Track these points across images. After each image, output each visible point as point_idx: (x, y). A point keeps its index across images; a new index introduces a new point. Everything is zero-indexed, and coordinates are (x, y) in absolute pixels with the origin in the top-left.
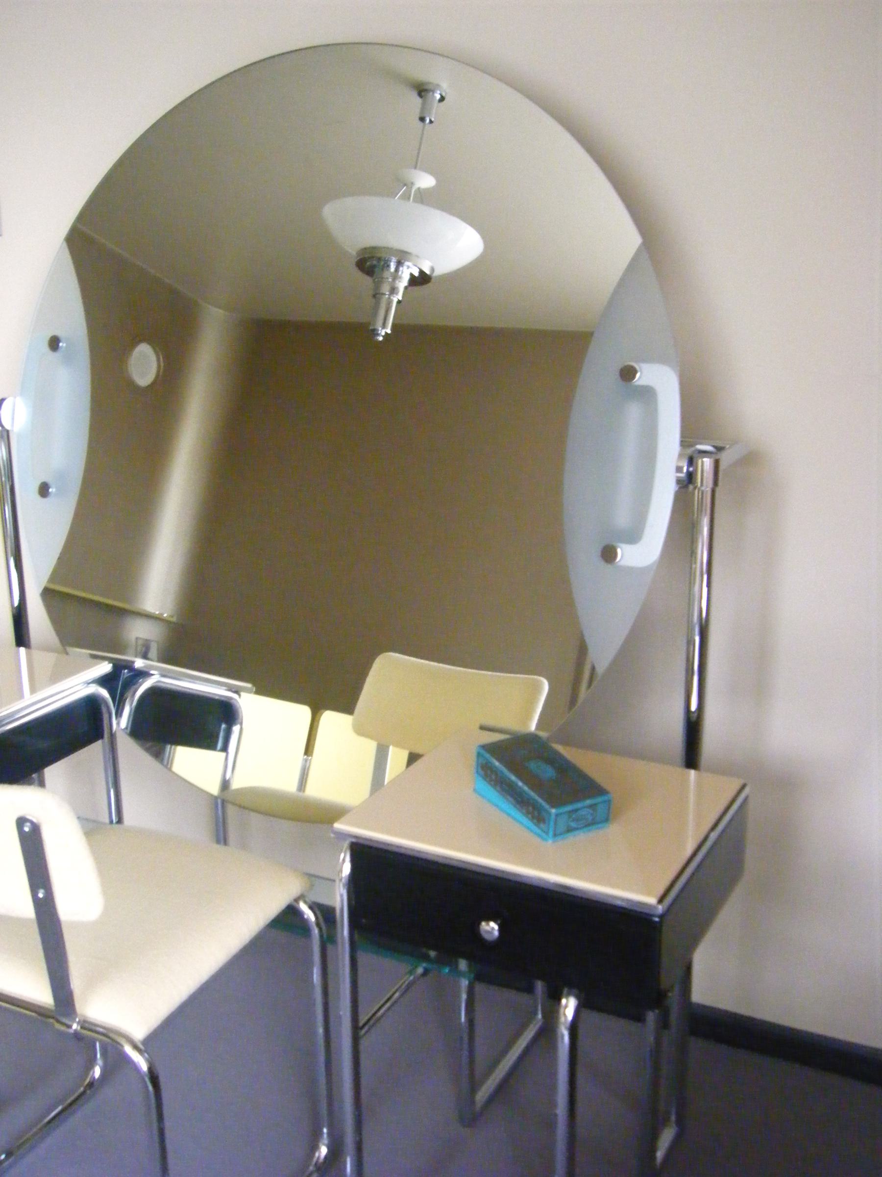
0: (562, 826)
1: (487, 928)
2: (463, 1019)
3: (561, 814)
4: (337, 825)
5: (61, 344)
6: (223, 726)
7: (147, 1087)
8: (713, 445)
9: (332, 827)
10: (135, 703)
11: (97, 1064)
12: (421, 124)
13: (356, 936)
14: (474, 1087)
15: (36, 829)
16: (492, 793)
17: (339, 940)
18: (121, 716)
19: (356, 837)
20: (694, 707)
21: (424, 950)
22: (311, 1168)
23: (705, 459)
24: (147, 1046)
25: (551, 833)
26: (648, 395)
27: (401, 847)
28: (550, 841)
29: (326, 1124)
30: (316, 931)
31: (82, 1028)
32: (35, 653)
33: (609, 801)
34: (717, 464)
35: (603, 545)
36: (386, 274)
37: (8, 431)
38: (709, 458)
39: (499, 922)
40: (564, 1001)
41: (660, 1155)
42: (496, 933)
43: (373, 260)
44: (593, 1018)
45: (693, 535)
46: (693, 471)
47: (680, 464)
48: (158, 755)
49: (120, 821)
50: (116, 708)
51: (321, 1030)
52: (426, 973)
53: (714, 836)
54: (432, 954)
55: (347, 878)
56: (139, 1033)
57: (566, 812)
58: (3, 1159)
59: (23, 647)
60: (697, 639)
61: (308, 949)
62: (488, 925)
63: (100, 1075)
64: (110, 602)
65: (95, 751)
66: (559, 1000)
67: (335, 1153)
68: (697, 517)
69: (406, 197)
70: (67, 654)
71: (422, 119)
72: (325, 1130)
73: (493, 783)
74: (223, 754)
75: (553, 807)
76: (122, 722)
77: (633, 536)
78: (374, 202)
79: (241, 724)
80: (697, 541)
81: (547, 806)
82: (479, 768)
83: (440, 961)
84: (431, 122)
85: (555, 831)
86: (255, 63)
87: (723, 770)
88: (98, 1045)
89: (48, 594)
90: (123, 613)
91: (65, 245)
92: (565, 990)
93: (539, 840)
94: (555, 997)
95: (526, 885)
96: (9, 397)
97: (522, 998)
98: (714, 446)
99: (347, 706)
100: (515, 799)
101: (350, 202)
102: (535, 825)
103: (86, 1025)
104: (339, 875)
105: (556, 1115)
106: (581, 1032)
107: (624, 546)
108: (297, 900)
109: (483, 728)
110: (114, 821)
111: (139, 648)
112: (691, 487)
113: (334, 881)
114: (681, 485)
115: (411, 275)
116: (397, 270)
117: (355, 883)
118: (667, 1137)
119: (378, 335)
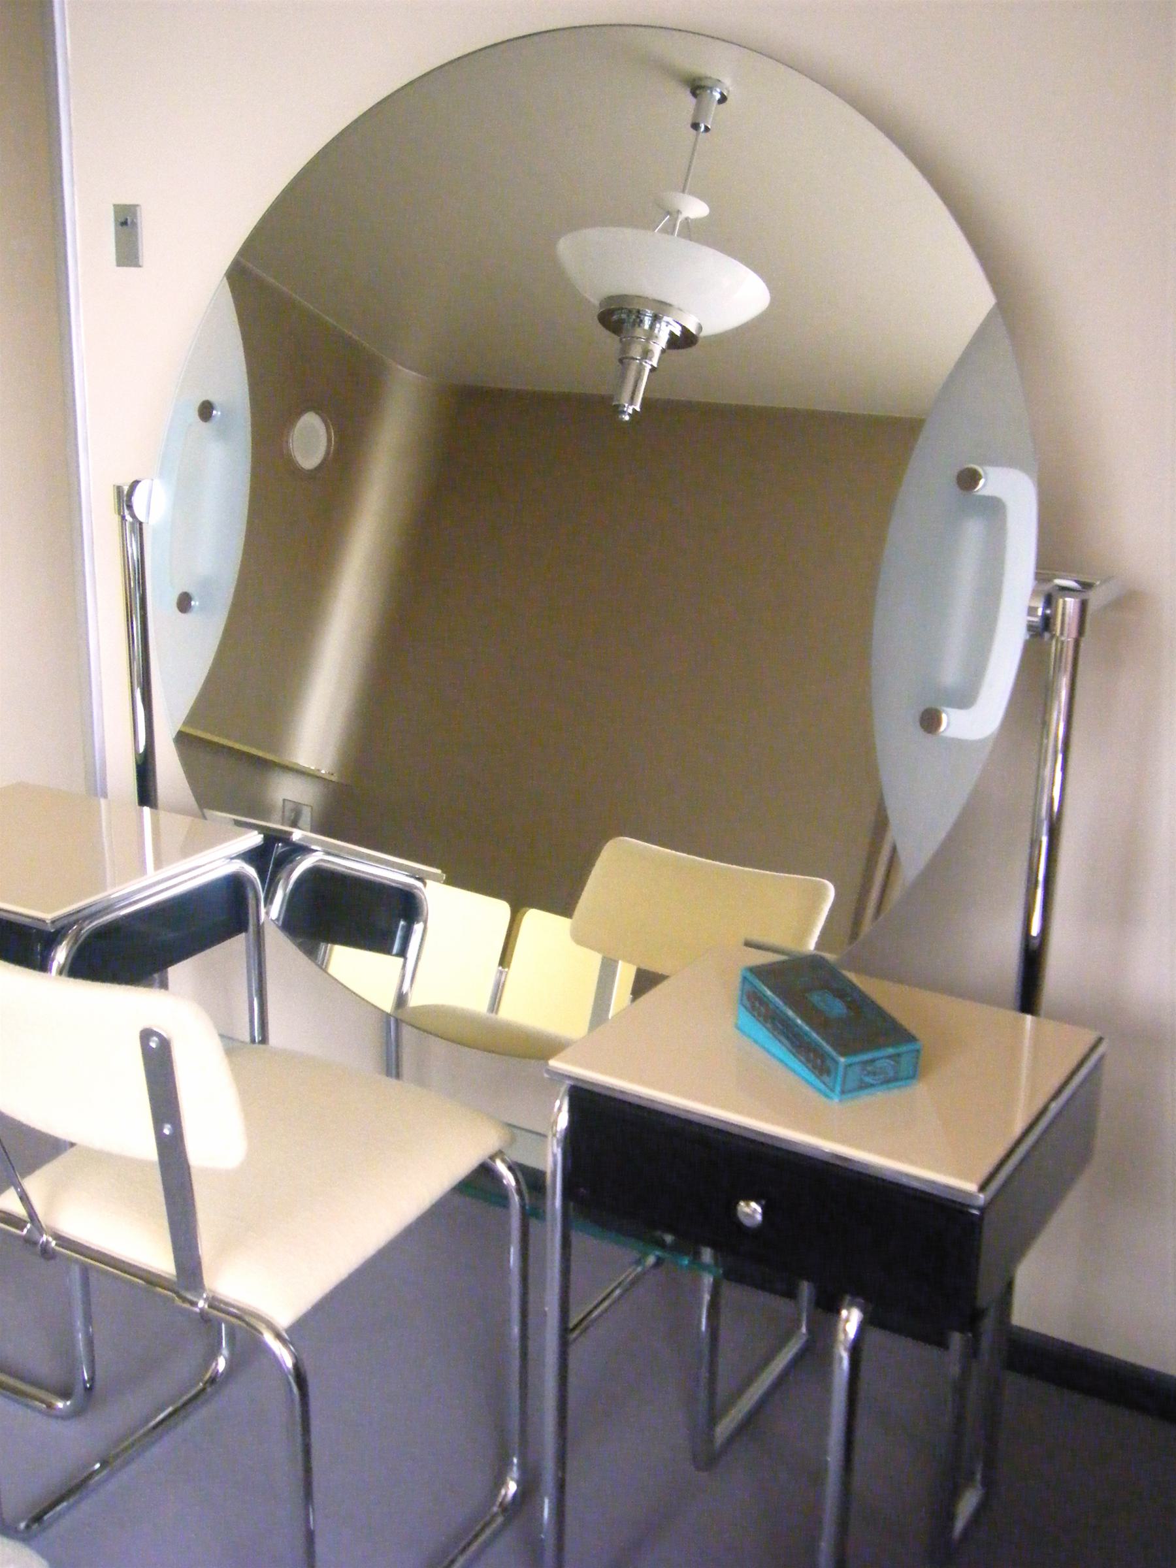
0: (850, 1084)
1: (747, 1210)
2: (703, 1328)
3: (855, 1064)
4: (553, 1063)
5: (214, 412)
6: (402, 923)
7: (291, 1391)
8: (1076, 579)
9: (547, 1064)
10: (290, 887)
11: (221, 1354)
12: (693, 132)
13: (572, 1212)
14: (713, 1418)
15: (165, 1044)
16: (762, 1033)
17: (549, 1217)
18: (271, 902)
19: (577, 1079)
20: (1035, 930)
21: (658, 1233)
22: (495, 1509)
23: (1067, 599)
24: (294, 1335)
25: (838, 1088)
26: (994, 508)
27: (614, 1089)
28: (836, 1100)
29: (517, 1452)
30: (516, 1199)
31: (210, 1306)
32: (162, 814)
33: (918, 1051)
34: (1083, 606)
35: (922, 708)
36: (638, 332)
37: (141, 524)
38: (1073, 598)
39: (763, 1202)
40: (844, 1313)
41: (960, 1525)
42: (759, 1217)
43: (622, 313)
44: (877, 1336)
45: (1046, 696)
46: (1051, 613)
47: (1033, 605)
48: (311, 952)
49: (264, 1040)
50: (265, 891)
51: (516, 1330)
52: (659, 1262)
53: (1055, 1107)
54: (669, 1238)
55: (563, 1133)
56: (284, 1318)
57: (859, 1063)
58: (97, 1470)
59: (147, 806)
60: (1045, 840)
61: (505, 1223)
62: (748, 1205)
63: (224, 1370)
64: (260, 754)
65: (238, 944)
66: (838, 1312)
67: (527, 1492)
68: (1053, 677)
69: (669, 230)
70: (204, 817)
71: (695, 126)
72: (515, 1460)
73: (761, 1019)
74: (401, 960)
75: (843, 1054)
76: (275, 910)
77: (965, 698)
78: (628, 233)
79: (425, 923)
80: (1051, 710)
81: (834, 1053)
82: (745, 998)
83: (676, 1249)
84: (707, 129)
85: (844, 1083)
86: (495, 45)
87: (1069, 1016)
88: (223, 1326)
89: (183, 740)
90: (264, 766)
91: (225, 278)
92: (848, 1298)
93: (824, 1099)
94: (829, 1306)
95: (796, 1154)
96: (143, 479)
97: (781, 1304)
98: (1076, 581)
99: (564, 906)
100: (792, 1043)
101: (593, 235)
102: (817, 1077)
103: (215, 1303)
104: (552, 1127)
105: (826, 1462)
106: (865, 1355)
107: (950, 710)
108: (492, 1158)
109: (748, 944)
110: (257, 1040)
111: (287, 814)
112: (1047, 635)
113: (545, 1136)
114: (1032, 633)
115: (672, 334)
116: (652, 327)
117: (574, 1140)
118: (968, 1503)
119: (624, 412)
